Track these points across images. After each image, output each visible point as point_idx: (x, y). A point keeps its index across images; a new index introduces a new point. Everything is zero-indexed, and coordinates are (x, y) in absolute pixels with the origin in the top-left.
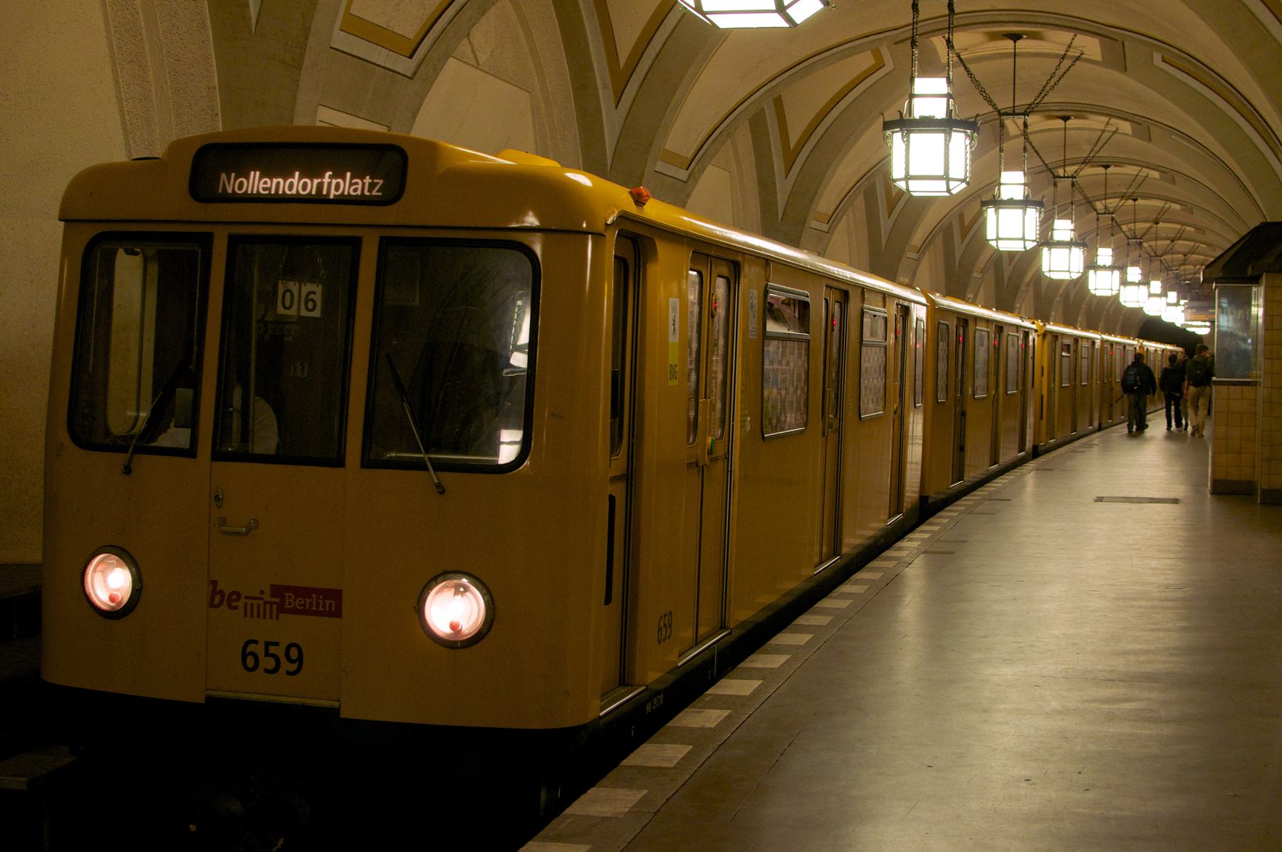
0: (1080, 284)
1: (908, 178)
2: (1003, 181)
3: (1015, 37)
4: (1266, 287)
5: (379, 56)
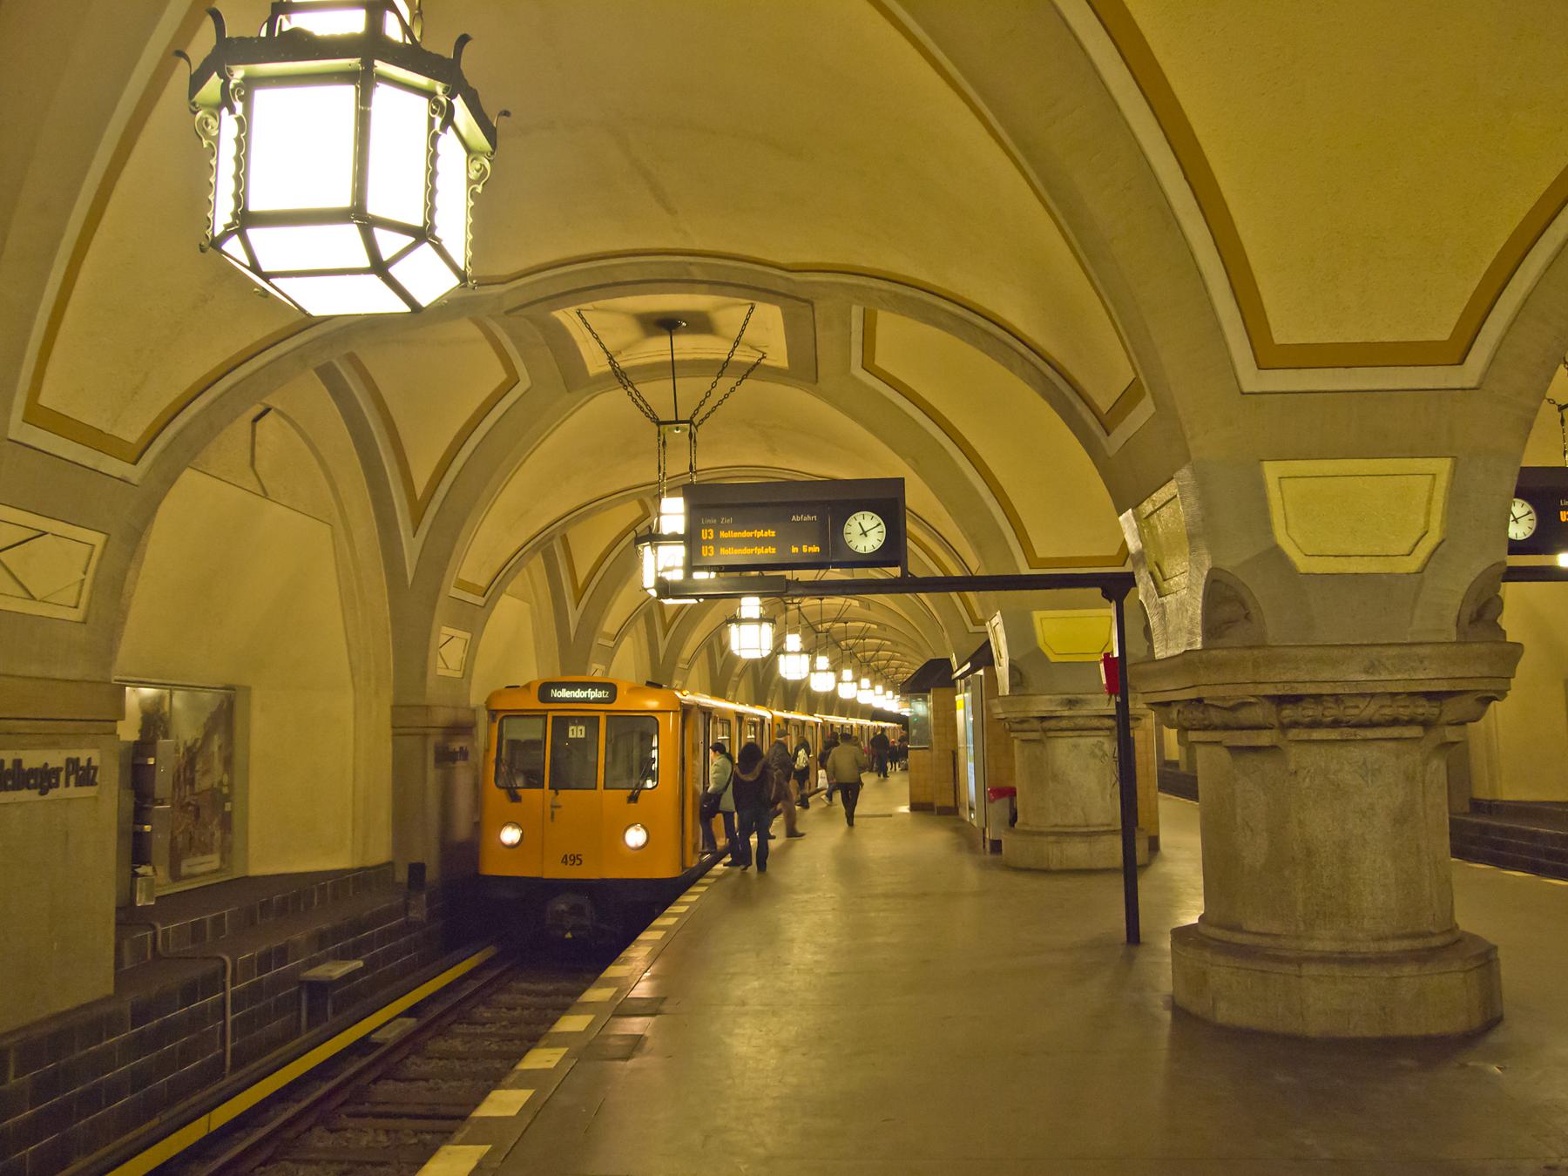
0: (834, 694)
1: (245, 220)
5: (470, 598)
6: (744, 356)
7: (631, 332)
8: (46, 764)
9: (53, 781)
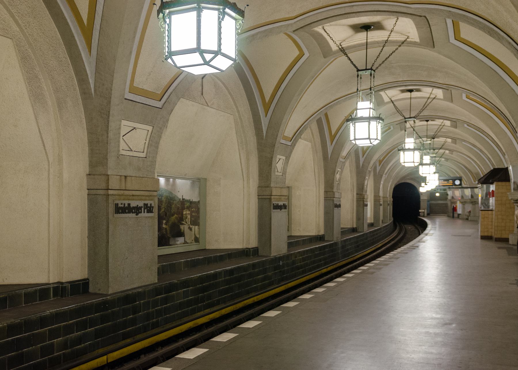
1: (355, 139)
2: (406, 142)
3: (411, 91)
4: (496, 186)
6: (446, 141)
7: (350, 32)
8: (138, 205)
9: (140, 211)
